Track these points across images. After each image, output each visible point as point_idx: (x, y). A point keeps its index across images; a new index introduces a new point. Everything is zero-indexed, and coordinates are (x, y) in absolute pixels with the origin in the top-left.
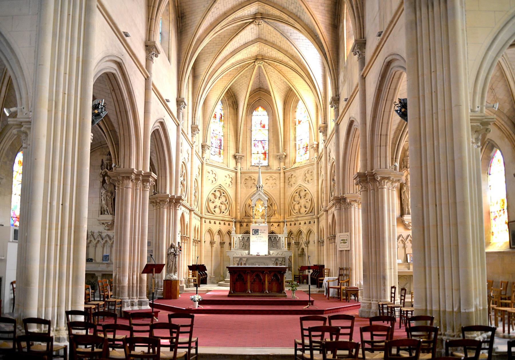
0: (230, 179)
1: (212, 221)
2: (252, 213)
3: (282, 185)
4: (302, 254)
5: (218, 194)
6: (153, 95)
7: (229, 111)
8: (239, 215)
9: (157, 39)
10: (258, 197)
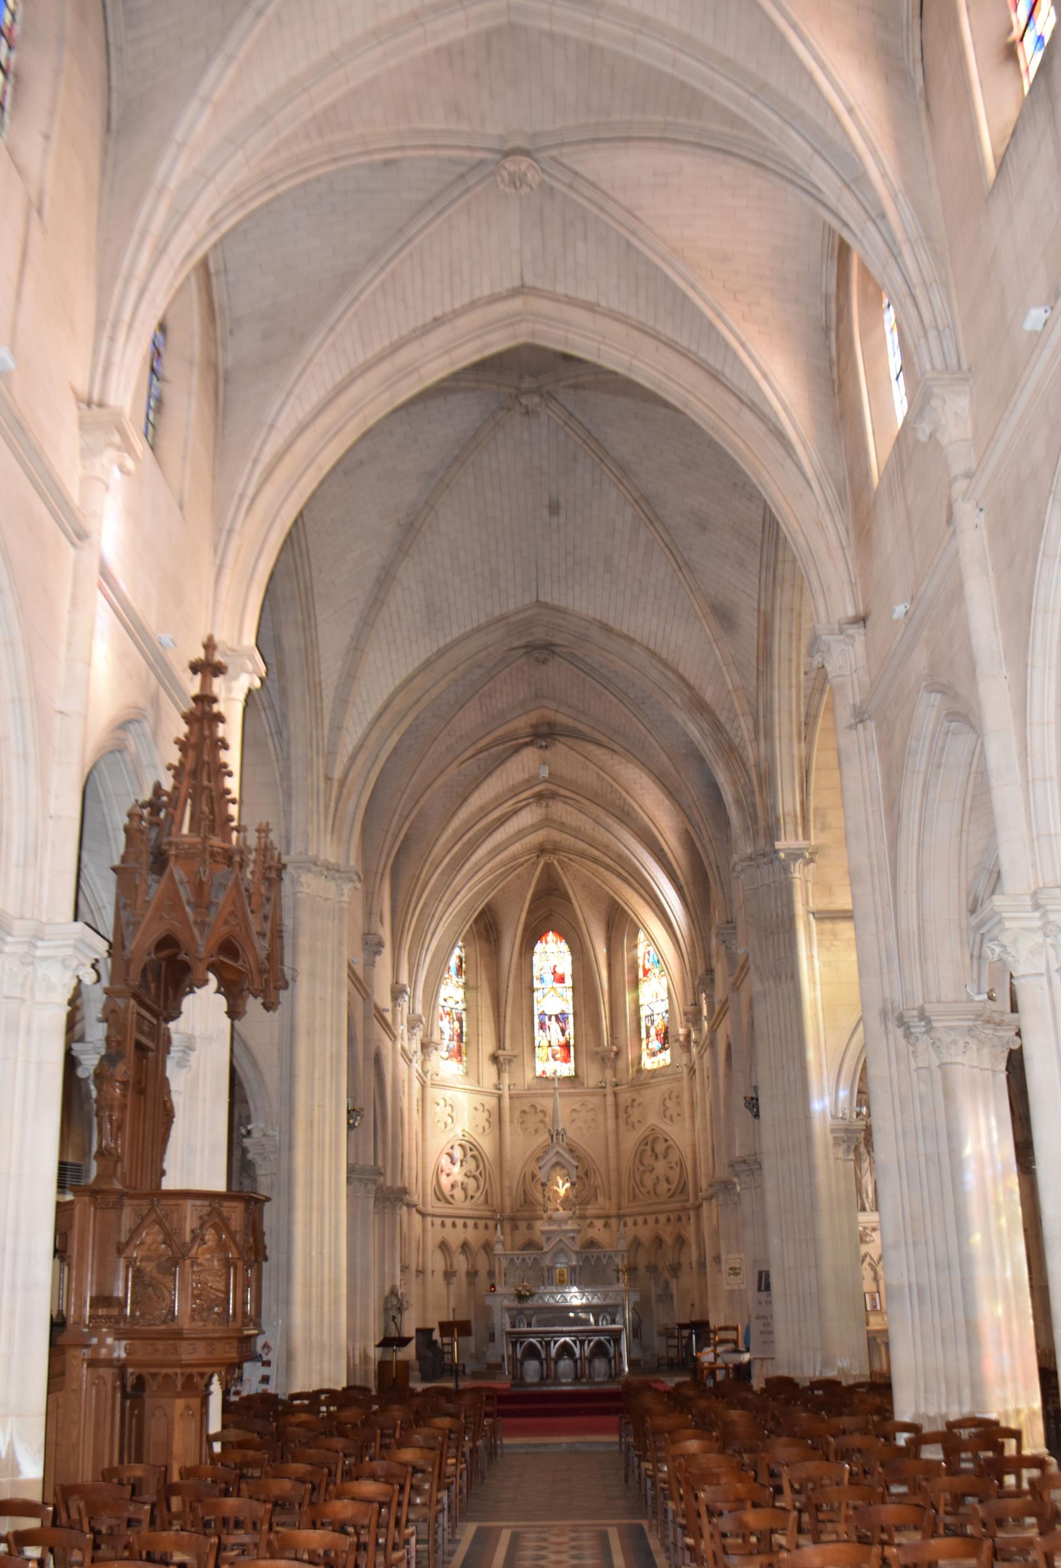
0: (486, 1115)
1: (448, 1222)
2: (539, 1196)
3: (611, 1124)
8: (508, 1203)
10: (554, 1160)
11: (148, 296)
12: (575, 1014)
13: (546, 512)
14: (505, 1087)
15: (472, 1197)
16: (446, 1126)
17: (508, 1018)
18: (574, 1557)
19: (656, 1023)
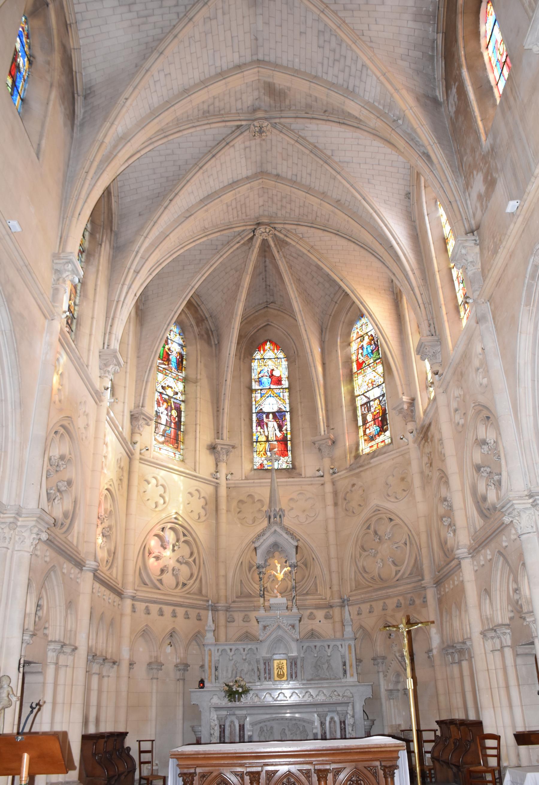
0: (202, 502)
1: (154, 608)
3: (330, 510)
10: (271, 541)
12: (291, 412)
14: (222, 475)
15: (184, 585)
16: (156, 507)
17: (226, 410)
19: (372, 410)
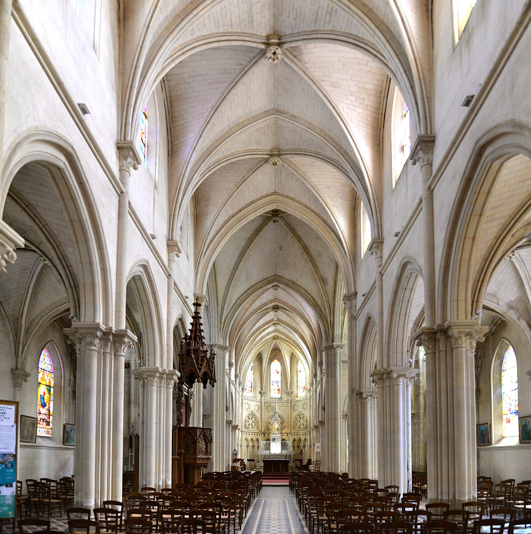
1: (248, 434)
3: (289, 410)
4: (301, 453)
5: (251, 417)
6: (129, 219)
7: (257, 363)
9: (177, 237)
11: (181, 207)
13: (279, 249)
18: (278, 528)
